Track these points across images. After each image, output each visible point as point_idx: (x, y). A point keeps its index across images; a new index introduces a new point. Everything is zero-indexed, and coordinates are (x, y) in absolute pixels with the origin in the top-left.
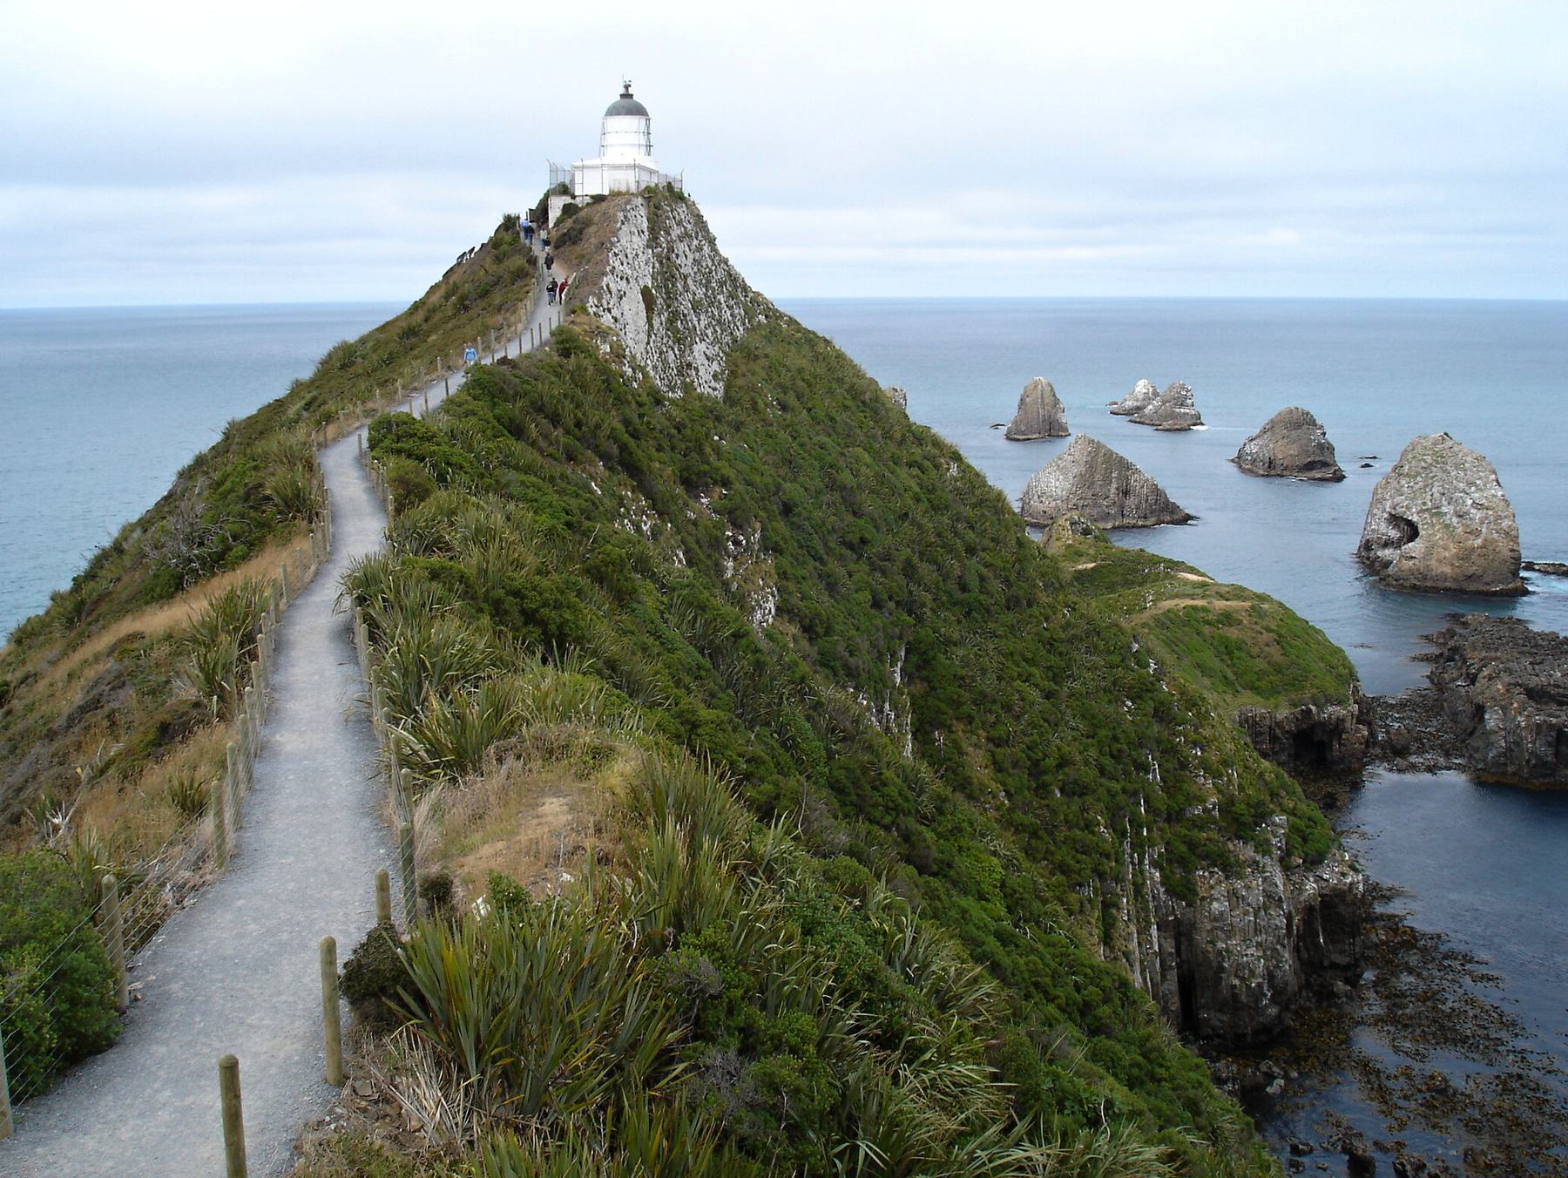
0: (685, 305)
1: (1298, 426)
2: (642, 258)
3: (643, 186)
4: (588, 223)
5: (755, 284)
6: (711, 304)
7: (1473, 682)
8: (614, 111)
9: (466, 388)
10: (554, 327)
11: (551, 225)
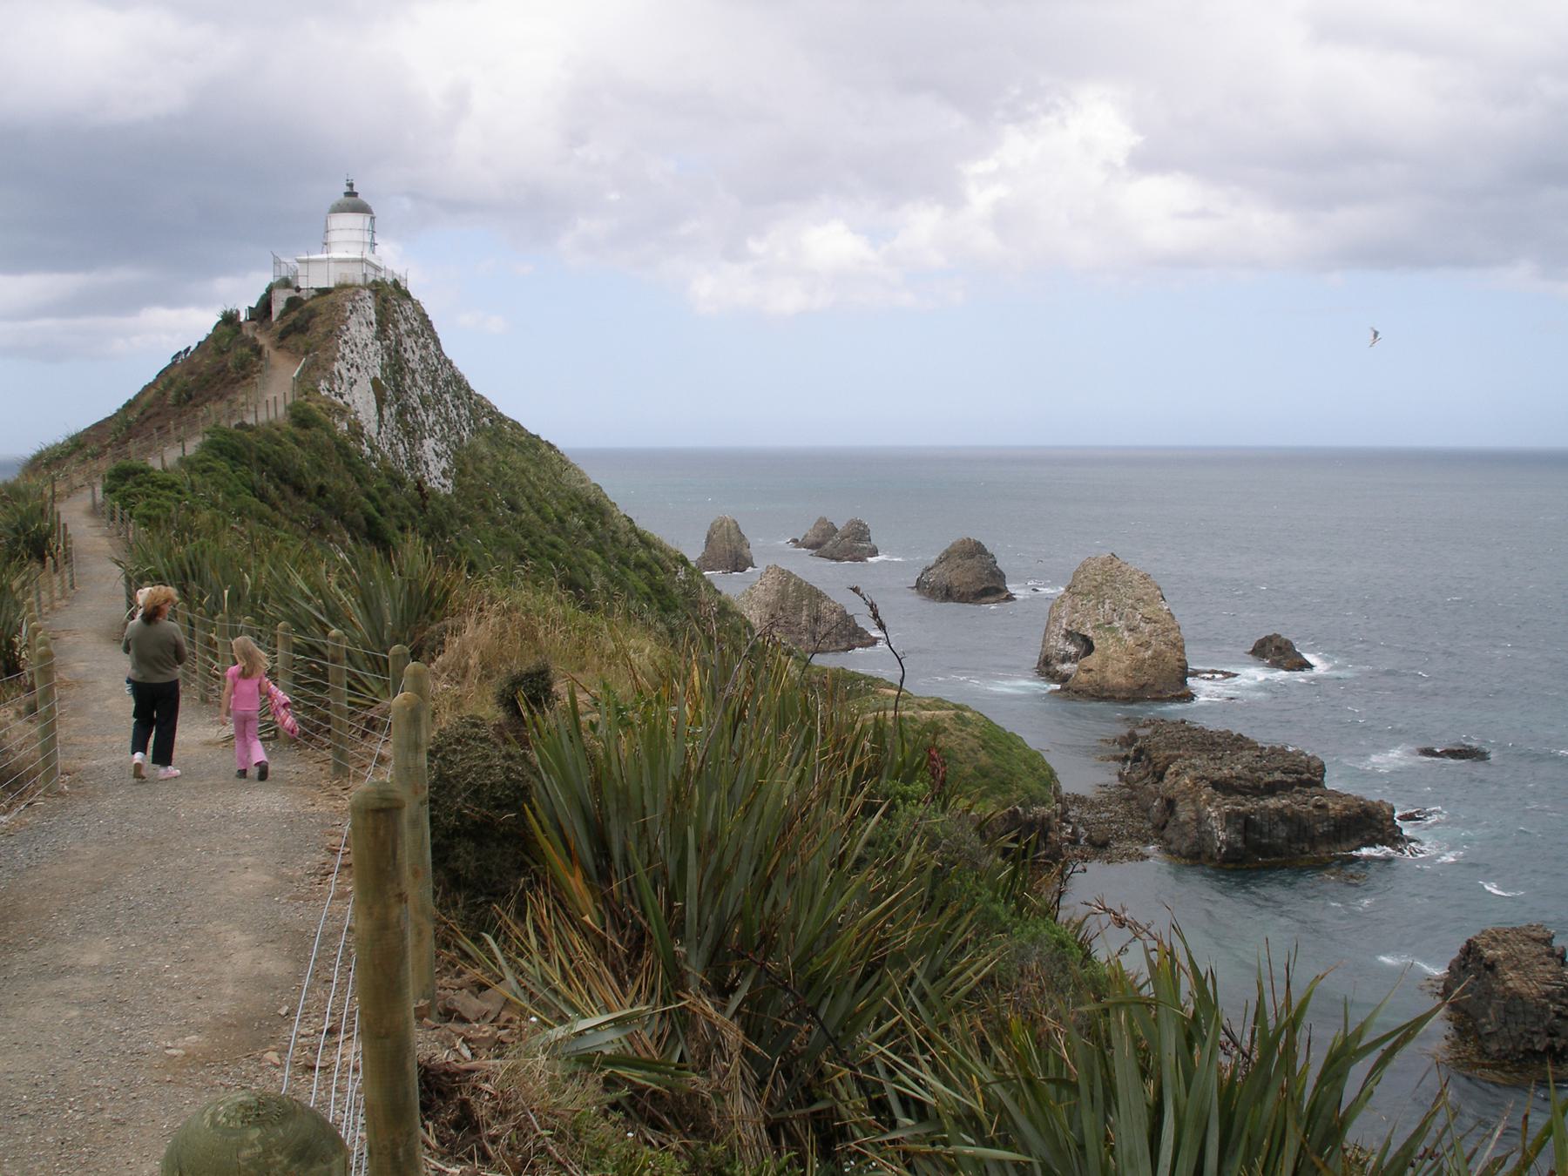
0: (414, 401)
1: (971, 555)
2: (371, 349)
3: (370, 279)
4: (313, 313)
5: (477, 386)
6: (438, 402)
7: (1161, 778)
8: (339, 209)
9: (205, 447)
10: (289, 401)
11: (274, 318)
